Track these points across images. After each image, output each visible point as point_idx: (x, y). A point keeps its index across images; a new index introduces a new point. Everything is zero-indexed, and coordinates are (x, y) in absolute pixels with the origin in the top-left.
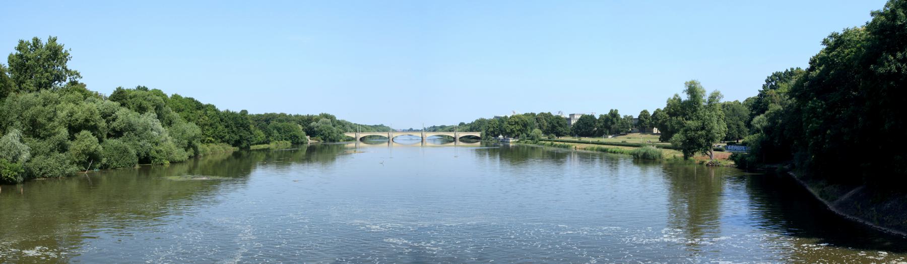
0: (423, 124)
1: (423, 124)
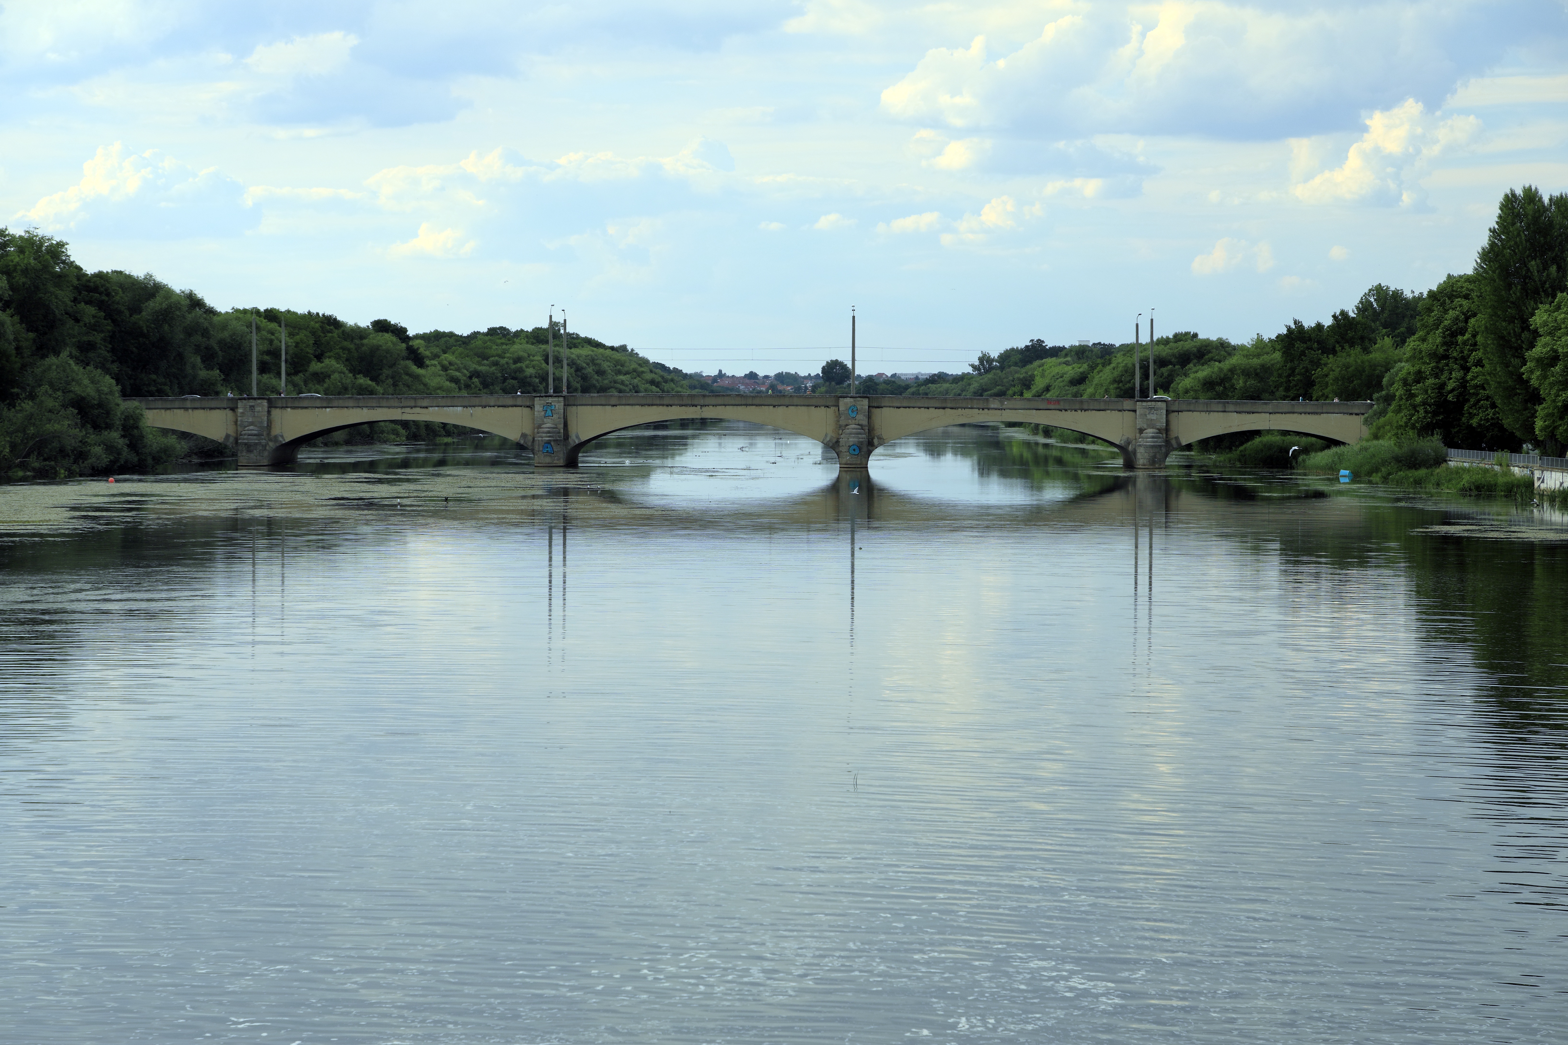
0: (551, 317)
1: (551, 317)
